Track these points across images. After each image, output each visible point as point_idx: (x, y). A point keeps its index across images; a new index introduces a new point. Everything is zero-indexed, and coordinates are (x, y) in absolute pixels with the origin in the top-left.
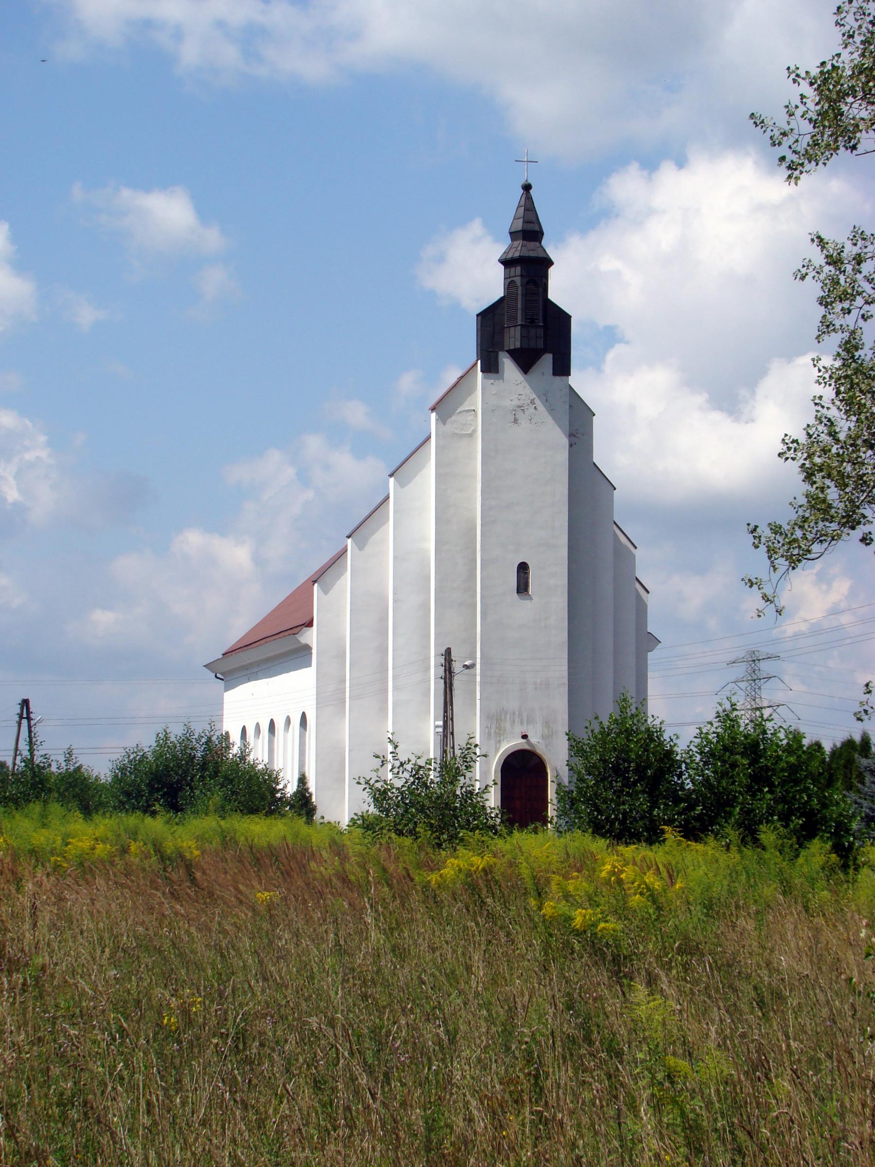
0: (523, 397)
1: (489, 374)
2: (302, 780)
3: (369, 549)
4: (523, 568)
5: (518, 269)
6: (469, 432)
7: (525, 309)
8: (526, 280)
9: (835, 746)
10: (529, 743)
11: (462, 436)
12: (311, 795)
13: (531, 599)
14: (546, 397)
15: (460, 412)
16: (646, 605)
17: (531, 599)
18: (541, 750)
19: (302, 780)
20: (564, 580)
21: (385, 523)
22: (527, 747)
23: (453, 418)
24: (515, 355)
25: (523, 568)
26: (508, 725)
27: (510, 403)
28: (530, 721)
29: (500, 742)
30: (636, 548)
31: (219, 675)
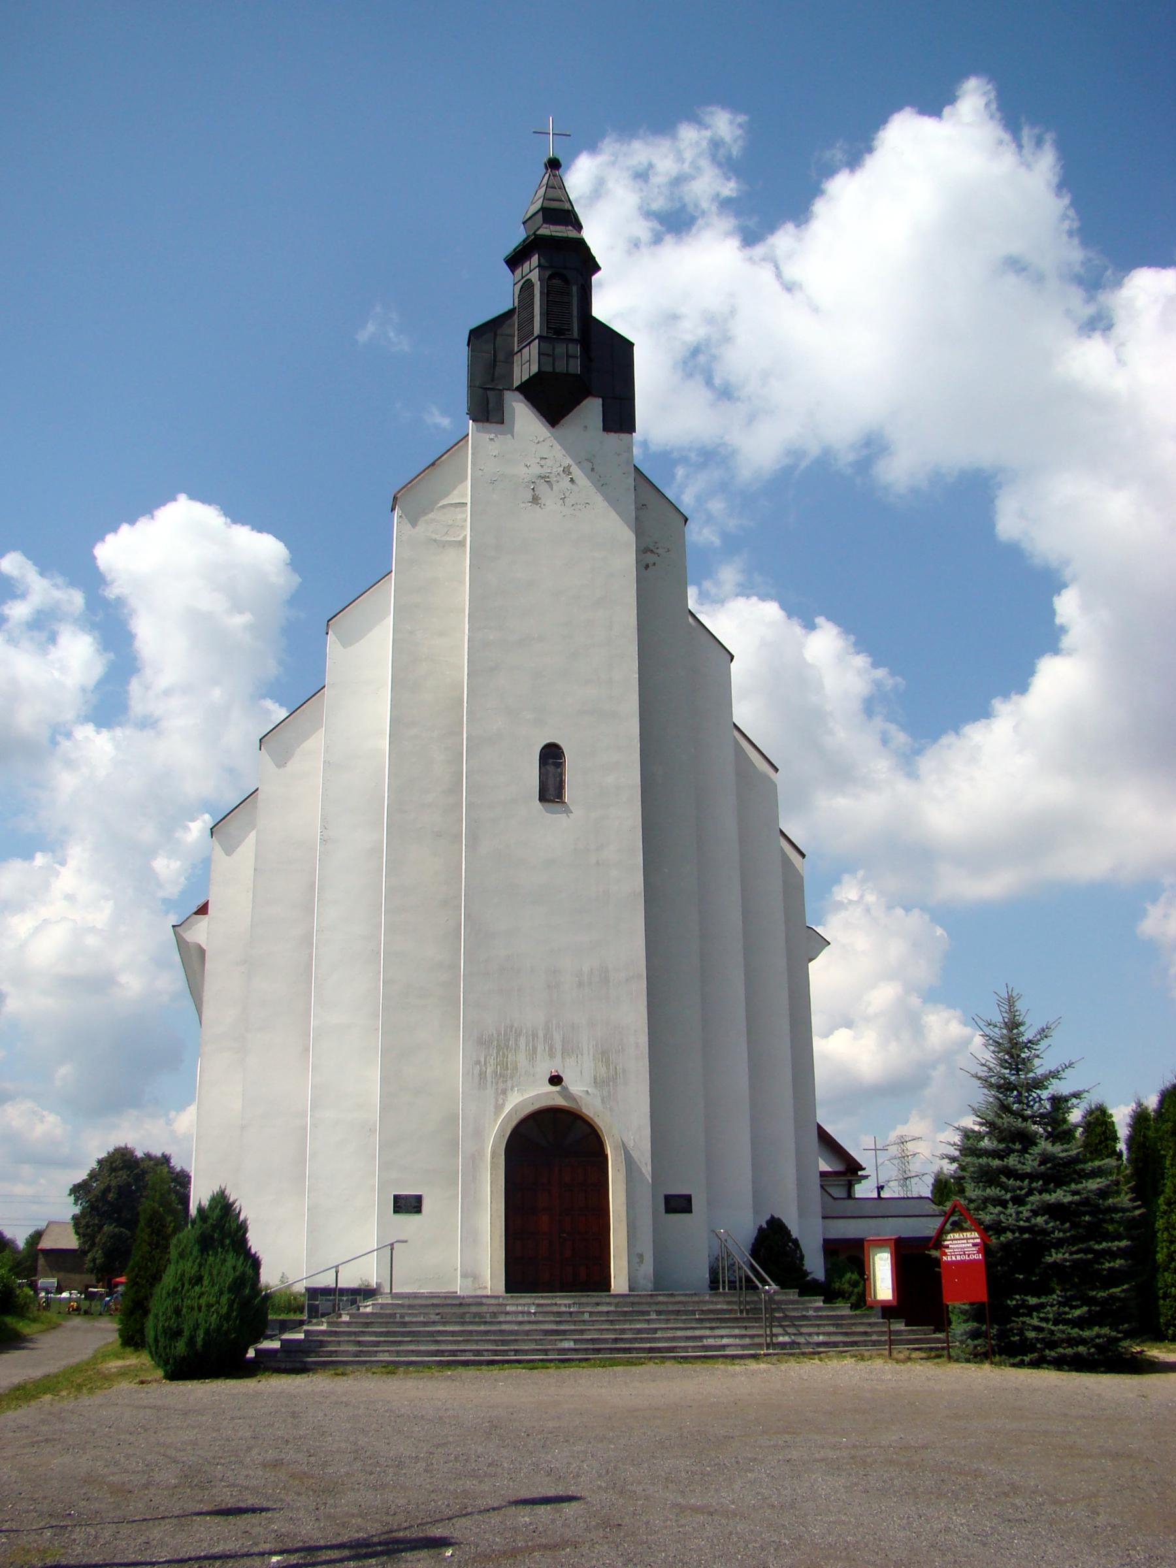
0: (549, 463)
1: (487, 425)
4: (551, 755)
5: (535, 260)
6: (460, 538)
7: (547, 315)
8: (548, 273)
10: (565, 1093)
13: (568, 811)
14: (591, 465)
15: (443, 507)
16: (802, 878)
17: (568, 811)
18: (593, 1107)
20: (633, 777)
22: (560, 1102)
23: (431, 516)
24: (533, 391)
25: (551, 755)
26: (522, 1059)
27: (524, 471)
28: (569, 1049)
29: (504, 1092)
30: (776, 770)
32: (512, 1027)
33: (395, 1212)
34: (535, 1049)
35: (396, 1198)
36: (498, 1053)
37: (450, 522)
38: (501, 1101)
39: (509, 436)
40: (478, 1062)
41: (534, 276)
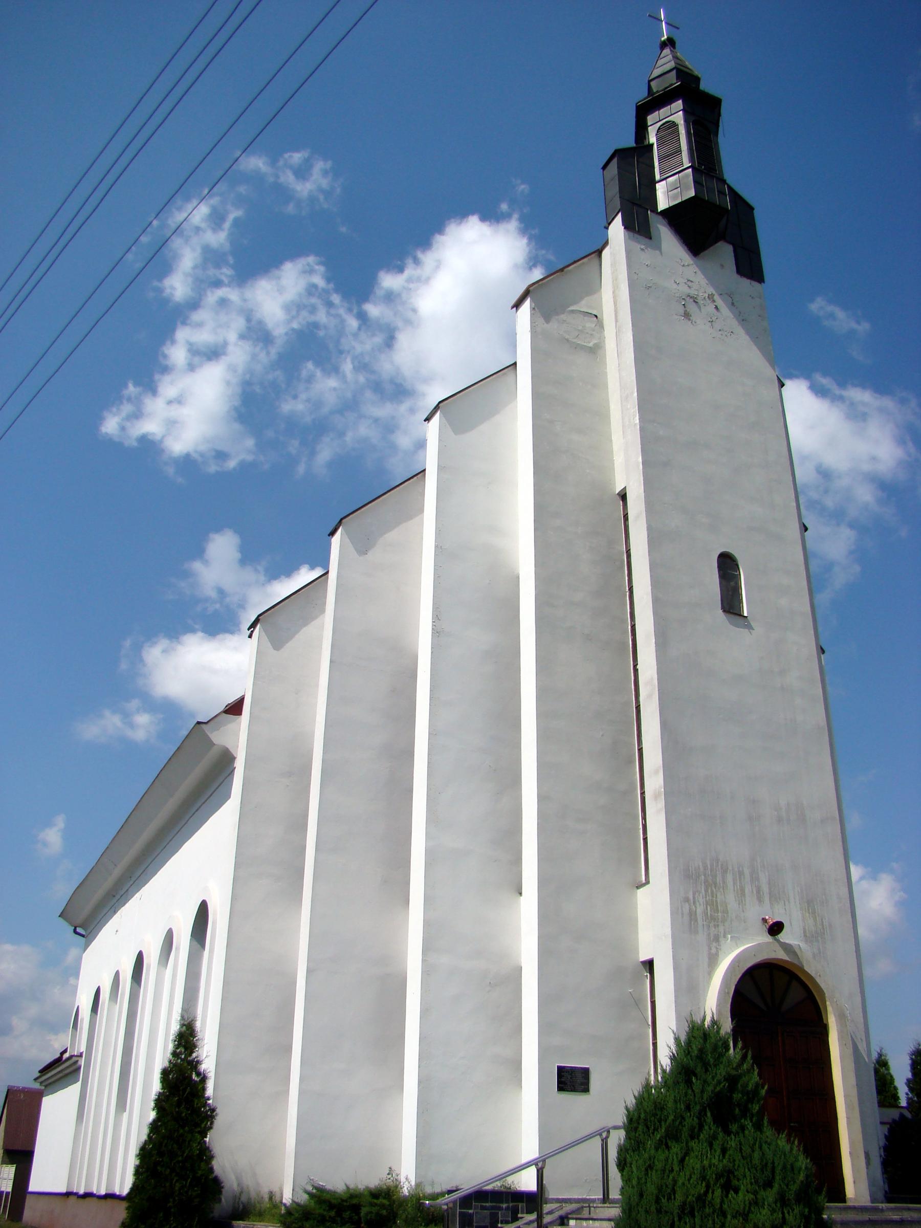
2: (186, 1039)
3: (376, 555)
4: (727, 565)
5: (679, 104)
6: (591, 345)
9: (647, 1086)
11: (578, 347)
12: (204, 1079)
15: (573, 311)
17: (749, 627)
19: (186, 1039)
21: (409, 517)
25: (727, 565)
26: (731, 899)
29: (717, 939)
31: (79, 930)
32: (718, 861)
33: (560, 1089)
34: (742, 890)
35: (561, 1070)
36: (706, 891)
37: (580, 328)
38: (714, 951)
39: (658, 252)
40: (687, 900)
41: (679, 118)
